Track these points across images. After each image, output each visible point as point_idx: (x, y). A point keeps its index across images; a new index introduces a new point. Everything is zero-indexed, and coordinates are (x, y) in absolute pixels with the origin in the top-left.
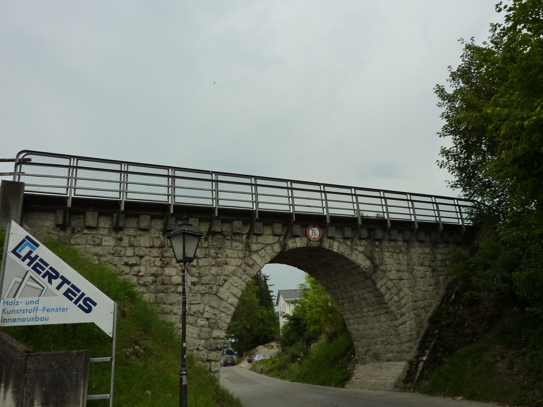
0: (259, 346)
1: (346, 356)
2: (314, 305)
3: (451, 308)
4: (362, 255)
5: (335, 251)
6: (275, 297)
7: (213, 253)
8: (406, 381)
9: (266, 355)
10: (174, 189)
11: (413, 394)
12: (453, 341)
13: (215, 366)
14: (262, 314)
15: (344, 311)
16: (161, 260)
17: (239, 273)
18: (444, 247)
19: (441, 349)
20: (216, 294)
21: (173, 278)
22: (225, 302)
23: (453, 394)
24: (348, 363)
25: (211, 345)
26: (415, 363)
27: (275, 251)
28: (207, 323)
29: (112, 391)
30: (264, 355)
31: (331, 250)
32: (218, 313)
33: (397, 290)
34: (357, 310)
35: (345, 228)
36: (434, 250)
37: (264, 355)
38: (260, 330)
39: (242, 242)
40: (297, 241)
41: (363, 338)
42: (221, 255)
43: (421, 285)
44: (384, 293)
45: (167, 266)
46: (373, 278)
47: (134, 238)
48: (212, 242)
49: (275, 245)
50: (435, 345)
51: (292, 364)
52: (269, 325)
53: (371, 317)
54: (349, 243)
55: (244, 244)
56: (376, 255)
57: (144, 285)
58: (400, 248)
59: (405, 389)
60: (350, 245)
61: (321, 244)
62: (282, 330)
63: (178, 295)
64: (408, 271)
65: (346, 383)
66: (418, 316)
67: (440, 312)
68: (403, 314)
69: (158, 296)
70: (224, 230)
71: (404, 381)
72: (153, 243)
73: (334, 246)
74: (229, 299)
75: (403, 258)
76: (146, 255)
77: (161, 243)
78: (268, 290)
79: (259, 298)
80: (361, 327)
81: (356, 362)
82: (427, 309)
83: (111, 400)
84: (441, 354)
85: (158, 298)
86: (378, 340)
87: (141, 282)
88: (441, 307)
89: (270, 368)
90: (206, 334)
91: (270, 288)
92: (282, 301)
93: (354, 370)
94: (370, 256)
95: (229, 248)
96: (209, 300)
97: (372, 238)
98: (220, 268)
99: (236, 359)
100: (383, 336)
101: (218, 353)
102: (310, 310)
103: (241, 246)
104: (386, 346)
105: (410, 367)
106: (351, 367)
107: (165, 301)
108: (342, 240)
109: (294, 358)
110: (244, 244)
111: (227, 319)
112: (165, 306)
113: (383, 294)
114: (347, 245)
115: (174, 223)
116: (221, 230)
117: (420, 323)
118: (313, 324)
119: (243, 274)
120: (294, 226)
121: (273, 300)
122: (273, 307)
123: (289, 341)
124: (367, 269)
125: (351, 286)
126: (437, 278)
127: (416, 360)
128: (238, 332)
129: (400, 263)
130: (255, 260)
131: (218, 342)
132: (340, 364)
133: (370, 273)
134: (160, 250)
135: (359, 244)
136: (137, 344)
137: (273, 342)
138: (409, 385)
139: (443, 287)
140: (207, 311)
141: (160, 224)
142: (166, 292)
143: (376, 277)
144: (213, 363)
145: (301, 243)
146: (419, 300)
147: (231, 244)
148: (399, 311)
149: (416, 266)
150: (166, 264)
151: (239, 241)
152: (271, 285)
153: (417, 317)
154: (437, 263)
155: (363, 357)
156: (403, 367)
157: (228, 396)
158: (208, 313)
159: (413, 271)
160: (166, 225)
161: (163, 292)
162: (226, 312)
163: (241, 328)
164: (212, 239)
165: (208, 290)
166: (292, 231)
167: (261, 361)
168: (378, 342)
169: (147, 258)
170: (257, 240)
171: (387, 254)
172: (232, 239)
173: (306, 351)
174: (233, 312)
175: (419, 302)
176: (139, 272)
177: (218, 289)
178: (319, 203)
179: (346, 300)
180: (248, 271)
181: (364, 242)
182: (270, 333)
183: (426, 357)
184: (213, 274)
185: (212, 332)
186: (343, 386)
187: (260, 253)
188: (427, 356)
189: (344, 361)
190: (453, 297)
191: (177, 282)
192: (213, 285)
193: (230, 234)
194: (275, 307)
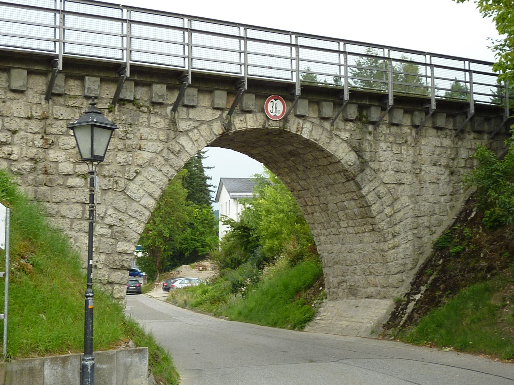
0: (183, 266)
1: (312, 288)
2: (273, 209)
3: (467, 230)
4: (346, 144)
5: (305, 136)
6: (215, 187)
7: (121, 131)
8: (387, 326)
9: (193, 281)
10: (64, 31)
11: (393, 342)
12: (459, 276)
13: (120, 291)
14: (189, 214)
15: (314, 223)
16: (42, 138)
17: (158, 163)
18: (474, 139)
19: (442, 286)
20: (123, 192)
21: (60, 165)
22: (136, 203)
23: (440, 344)
24: (313, 298)
25: (114, 262)
26: (404, 303)
27: (213, 132)
28: (110, 231)
29: (6, 311)
30: (190, 281)
31: (300, 135)
32: (125, 218)
33: (392, 199)
34: (332, 223)
35: (324, 103)
36: (457, 143)
37: (190, 280)
38: (186, 239)
39: (164, 117)
40: (248, 119)
41: (337, 263)
42: (132, 135)
43: (429, 194)
44: (372, 203)
45: (52, 147)
46: (358, 180)
47: (3, 104)
48: (120, 116)
49: (215, 123)
50: (435, 280)
51: (232, 295)
52: (202, 234)
53: (351, 235)
54: (327, 125)
55: (167, 121)
56: (366, 146)
57: (19, 174)
58: (405, 138)
59: (384, 336)
60: (329, 130)
61: (284, 125)
62: (221, 243)
63: (68, 190)
64: (412, 172)
65: (306, 324)
66: (418, 237)
67: (450, 234)
68: (396, 234)
69: (38, 190)
70: (138, 98)
71: (384, 326)
72: (31, 112)
73: (304, 130)
74: (143, 200)
75: (408, 153)
76: (21, 129)
77: (44, 112)
78: (203, 175)
79: (187, 188)
80: (336, 248)
81: (324, 297)
82: (433, 229)
83: (5, 320)
84: (440, 293)
85: (38, 193)
86: (357, 267)
87: (15, 169)
88: (454, 228)
89: (199, 300)
90: (107, 246)
91: (207, 173)
92: (225, 195)
93: (321, 307)
94: (358, 147)
95: (144, 124)
96: (114, 200)
97: (364, 119)
98: (131, 155)
99: (144, 284)
100: (365, 262)
101: (124, 274)
102: (268, 217)
103: (162, 123)
104: (367, 277)
105: (397, 308)
106: (317, 303)
107: (49, 197)
108: (317, 121)
109: (236, 287)
110: (167, 121)
111: (138, 228)
112: (48, 205)
113: (370, 204)
114: (324, 129)
115: (62, 84)
116: (134, 98)
117: (420, 248)
118: (271, 238)
119: (164, 165)
120: (246, 96)
121: (211, 193)
122: (211, 204)
123: (232, 260)
124: (350, 165)
125: (325, 189)
126: (456, 184)
127: (406, 299)
128: (149, 242)
129: (402, 159)
130: (183, 144)
131: (124, 258)
132: (301, 299)
133: (354, 173)
134: (42, 124)
135: (343, 127)
136: (23, 258)
137: (207, 260)
138: (390, 332)
139: (462, 198)
140: (110, 215)
141: (41, 84)
142: (50, 184)
143: (362, 178)
144: (116, 286)
145: (255, 122)
146: (423, 214)
147: (149, 119)
148: (390, 229)
149: (426, 165)
150: (50, 145)
151: (160, 115)
152: (208, 168)
153: (417, 239)
154: (458, 163)
155: (335, 290)
156: (386, 307)
157: (137, 329)
158: (112, 217)
159: (420, 173)
160: (51, 85)
161: (45, 185)
162: (138, 217)
163: (154, 235)
164: (119, 111)
165: (113, 185)
166: (242, 103)
167: (185, 288)
168: (357, 271)
169: (22, 133)
170: (188, 114)
171: (383, 145)
172: (150, 111)
173: (255, 277)
174: (147, 217)
175: (422, 218)
176: (10, 154)
177: (127, 184)
178: (286, 64)
179: (317, 208)
180: (172, 160)
181: (350, 126)
182: (203, 246)
183: (420, 295)
184: (120, 163)
185: (116, 245)
186: (301, 329)
187: (191, 134)
188: (422, 294)
189: (309, 294)
190: (473, 215)
191: (66, 171)
192: (120, 179)
193: (148, 104)
194: (213, 204)
